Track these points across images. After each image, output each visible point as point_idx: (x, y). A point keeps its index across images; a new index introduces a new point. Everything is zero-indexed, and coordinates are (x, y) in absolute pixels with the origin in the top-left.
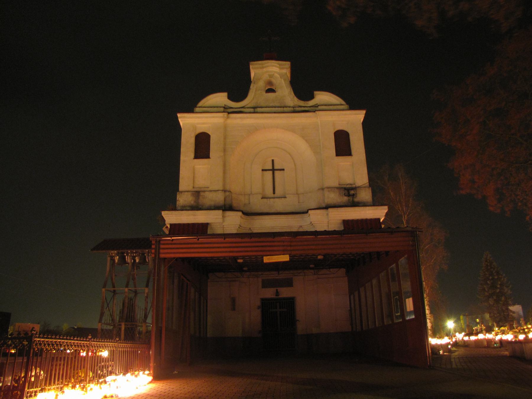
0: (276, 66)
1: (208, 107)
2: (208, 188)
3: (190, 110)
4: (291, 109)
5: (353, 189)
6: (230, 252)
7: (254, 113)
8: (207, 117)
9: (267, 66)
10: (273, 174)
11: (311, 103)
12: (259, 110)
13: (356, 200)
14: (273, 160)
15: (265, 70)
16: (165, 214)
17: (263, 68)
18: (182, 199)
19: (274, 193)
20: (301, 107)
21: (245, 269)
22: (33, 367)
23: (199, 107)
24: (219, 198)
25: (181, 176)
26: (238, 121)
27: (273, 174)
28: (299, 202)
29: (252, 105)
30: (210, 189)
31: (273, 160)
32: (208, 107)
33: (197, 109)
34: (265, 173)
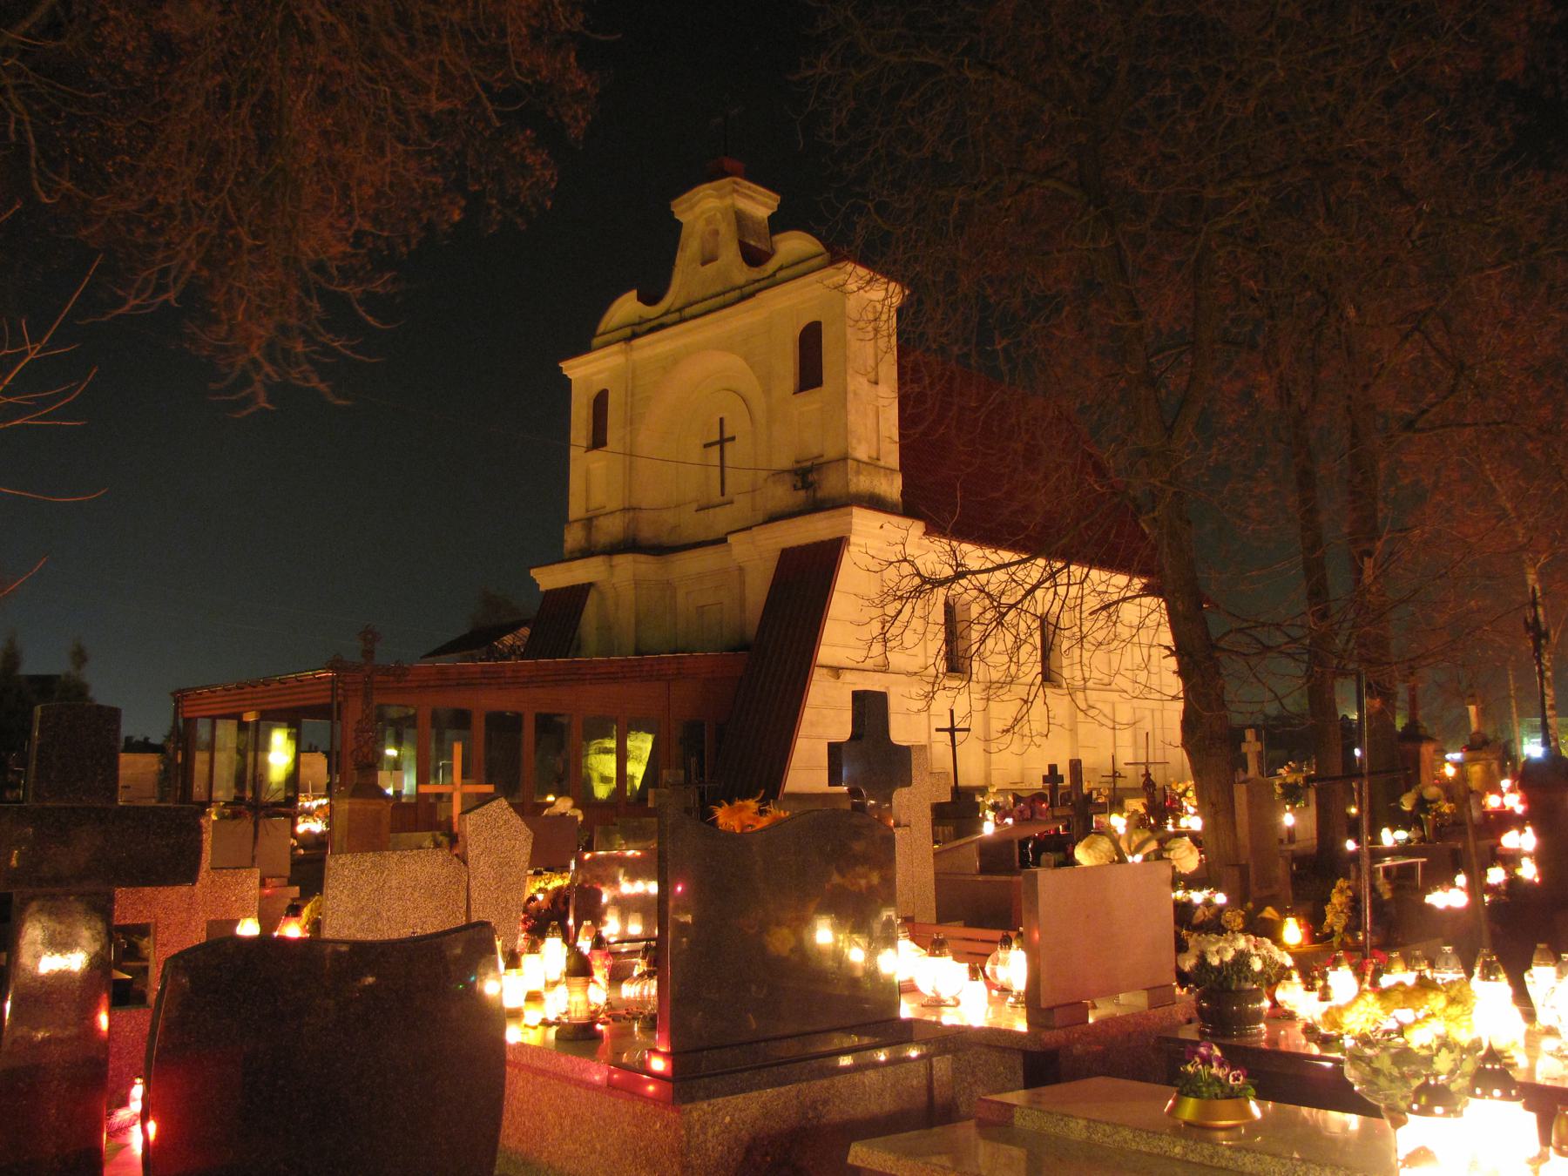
0: (710, 196)
1: (617, 330)
2: (604, 507)
3: (581, 346)
4: (736, 294)
5: (810, 470)
6: (233, 707)
7: (683, 320)
8: (596, 360)
9: (699, 201)
10: (722, 450)
11: (771, 267)
12: (688, 312)
13: (819, 494)
14: (722, 420)
15: (697, 210)
16: (535, 573)
17: (691, 208)
18: (573, 537)
19: (723, 494)
20: (758, 281)
21: (204, 737)
22: (1067, 781)
23: (600, 335)
24: (612, 528)
25: (571, 491)
26: (647, 353)
27: (722, 450)
28: (753, 510)
29: (678, 304)
30: (608, 509)
31: (722, 420)
32: (617, 330)
33: (596, 341)
34: (710, 449)
